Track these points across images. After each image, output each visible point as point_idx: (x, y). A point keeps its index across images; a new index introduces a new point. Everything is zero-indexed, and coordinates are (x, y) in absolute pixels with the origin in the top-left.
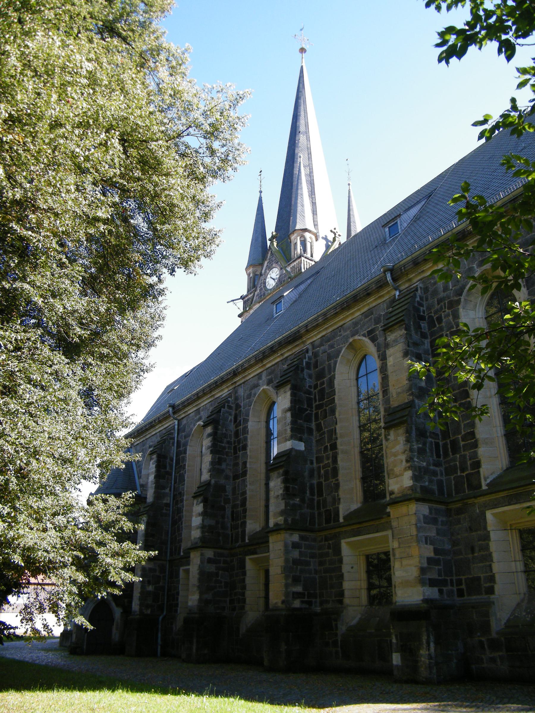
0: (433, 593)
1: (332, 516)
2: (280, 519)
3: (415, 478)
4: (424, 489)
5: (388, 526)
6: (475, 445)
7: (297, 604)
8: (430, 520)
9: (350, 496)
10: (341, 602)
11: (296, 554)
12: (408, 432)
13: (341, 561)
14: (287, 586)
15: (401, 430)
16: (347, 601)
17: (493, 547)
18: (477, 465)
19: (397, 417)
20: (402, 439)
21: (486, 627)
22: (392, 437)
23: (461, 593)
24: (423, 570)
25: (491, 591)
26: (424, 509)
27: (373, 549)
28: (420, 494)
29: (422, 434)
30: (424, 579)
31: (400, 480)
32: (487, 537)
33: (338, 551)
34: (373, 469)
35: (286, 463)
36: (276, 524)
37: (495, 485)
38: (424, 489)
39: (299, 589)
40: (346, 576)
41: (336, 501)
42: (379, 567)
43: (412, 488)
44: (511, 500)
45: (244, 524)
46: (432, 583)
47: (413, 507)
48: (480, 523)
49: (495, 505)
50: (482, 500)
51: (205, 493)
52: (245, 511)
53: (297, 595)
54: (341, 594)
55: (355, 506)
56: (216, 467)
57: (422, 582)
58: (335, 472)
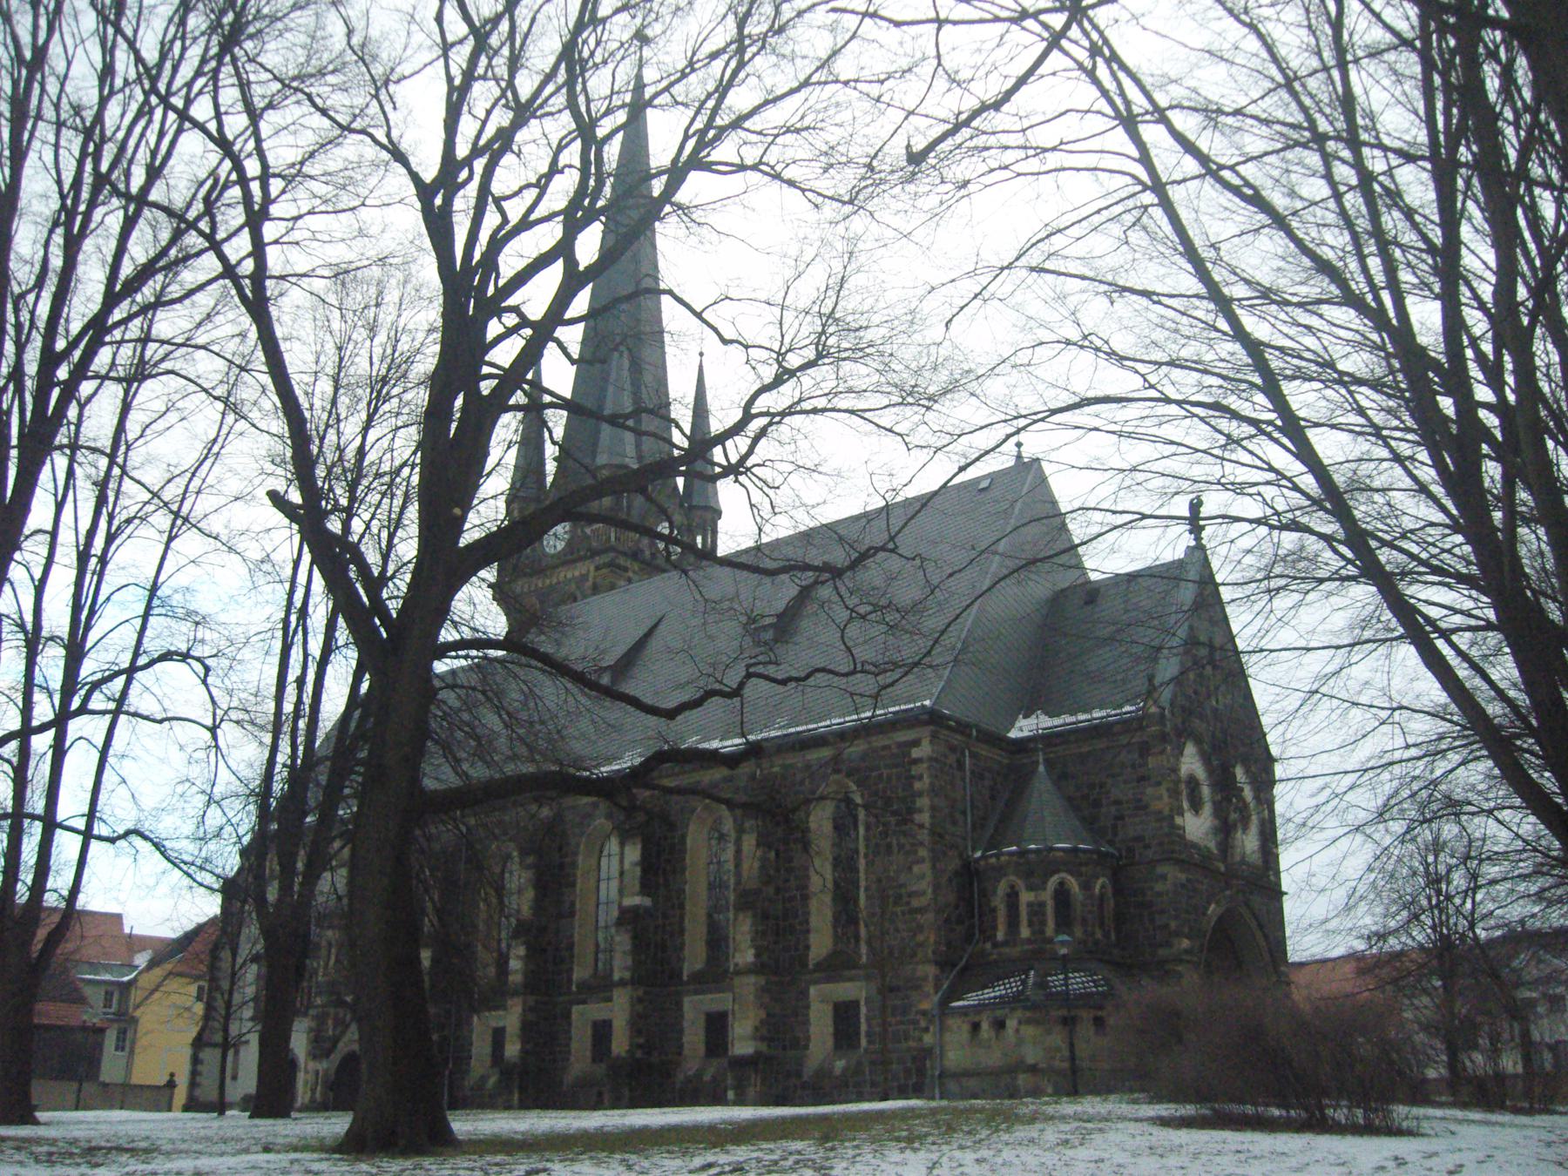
0: (763, 1047)
1: (676, 975)
2: (627, 975)
3: (757, 955)
4: (763, 965)
5: (731, 989)
6: (808, 931)
7: (639, 1054)
8: (764, 990)
9: (694, 957)
10: (680, 1054)
11: (640, 1008)
12: (754, 916)
13: (682, 1016)
14: (631, 1038)
15: (750, 913)
16: (686, 1052)
17: (812, 1015)
18: (808, 947)
19: (747, 901)
20: (749, 921)
21: (799, 1074)
22: (741, 917)
23: (784, 1048)
24: (756, 1029)
25: (806, 1047)
26: (762, 980)
27: (715, 1007)
28: (758, 968)
29: (766, 916)
30: (757, 1035)
31: (745, 956)
32: (808, 1007)
33: (679, 1005)
34: (717, 942)
35: (629, 918)
36: (621, 979)
37: (819, 966)
38: (763, 965)
39: (641, 1041)
40: (687, 1031)
41: (681, 960)
42: (717, 1025)
43: (754, 964)
44: (828, 980)
45: (571, 970)
46: (762, 1039)
47: (752, 979)
48: (804, 994)
49: (816, 982)
50: (808, 977)
51: (521, 930)
52: (572, 956)
53: (640, 1046)
54: (681, 1047)
55: (699, 966)
56: (538, 906)
57: (755, 1039)
58: (682, 931)
